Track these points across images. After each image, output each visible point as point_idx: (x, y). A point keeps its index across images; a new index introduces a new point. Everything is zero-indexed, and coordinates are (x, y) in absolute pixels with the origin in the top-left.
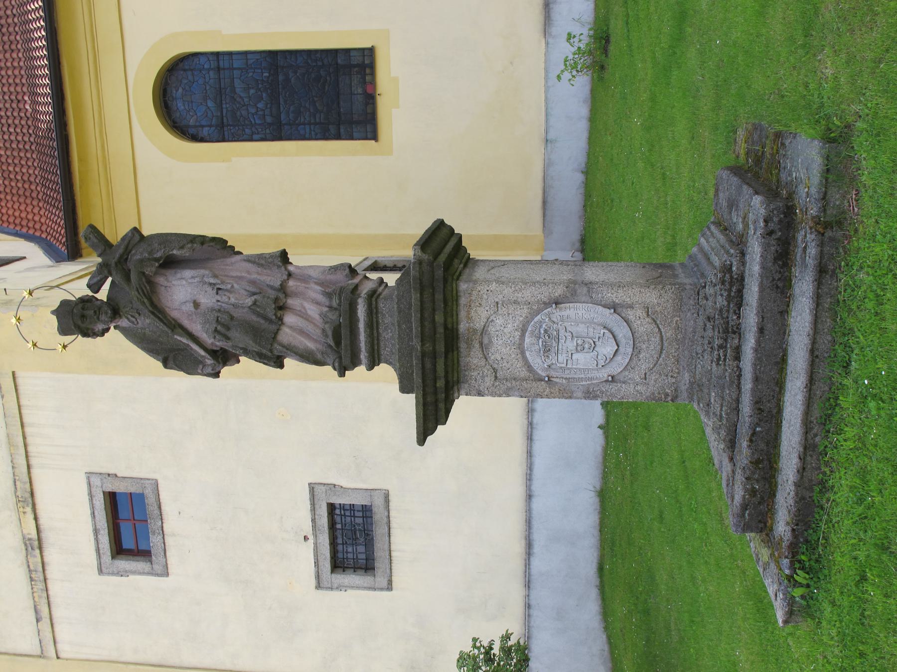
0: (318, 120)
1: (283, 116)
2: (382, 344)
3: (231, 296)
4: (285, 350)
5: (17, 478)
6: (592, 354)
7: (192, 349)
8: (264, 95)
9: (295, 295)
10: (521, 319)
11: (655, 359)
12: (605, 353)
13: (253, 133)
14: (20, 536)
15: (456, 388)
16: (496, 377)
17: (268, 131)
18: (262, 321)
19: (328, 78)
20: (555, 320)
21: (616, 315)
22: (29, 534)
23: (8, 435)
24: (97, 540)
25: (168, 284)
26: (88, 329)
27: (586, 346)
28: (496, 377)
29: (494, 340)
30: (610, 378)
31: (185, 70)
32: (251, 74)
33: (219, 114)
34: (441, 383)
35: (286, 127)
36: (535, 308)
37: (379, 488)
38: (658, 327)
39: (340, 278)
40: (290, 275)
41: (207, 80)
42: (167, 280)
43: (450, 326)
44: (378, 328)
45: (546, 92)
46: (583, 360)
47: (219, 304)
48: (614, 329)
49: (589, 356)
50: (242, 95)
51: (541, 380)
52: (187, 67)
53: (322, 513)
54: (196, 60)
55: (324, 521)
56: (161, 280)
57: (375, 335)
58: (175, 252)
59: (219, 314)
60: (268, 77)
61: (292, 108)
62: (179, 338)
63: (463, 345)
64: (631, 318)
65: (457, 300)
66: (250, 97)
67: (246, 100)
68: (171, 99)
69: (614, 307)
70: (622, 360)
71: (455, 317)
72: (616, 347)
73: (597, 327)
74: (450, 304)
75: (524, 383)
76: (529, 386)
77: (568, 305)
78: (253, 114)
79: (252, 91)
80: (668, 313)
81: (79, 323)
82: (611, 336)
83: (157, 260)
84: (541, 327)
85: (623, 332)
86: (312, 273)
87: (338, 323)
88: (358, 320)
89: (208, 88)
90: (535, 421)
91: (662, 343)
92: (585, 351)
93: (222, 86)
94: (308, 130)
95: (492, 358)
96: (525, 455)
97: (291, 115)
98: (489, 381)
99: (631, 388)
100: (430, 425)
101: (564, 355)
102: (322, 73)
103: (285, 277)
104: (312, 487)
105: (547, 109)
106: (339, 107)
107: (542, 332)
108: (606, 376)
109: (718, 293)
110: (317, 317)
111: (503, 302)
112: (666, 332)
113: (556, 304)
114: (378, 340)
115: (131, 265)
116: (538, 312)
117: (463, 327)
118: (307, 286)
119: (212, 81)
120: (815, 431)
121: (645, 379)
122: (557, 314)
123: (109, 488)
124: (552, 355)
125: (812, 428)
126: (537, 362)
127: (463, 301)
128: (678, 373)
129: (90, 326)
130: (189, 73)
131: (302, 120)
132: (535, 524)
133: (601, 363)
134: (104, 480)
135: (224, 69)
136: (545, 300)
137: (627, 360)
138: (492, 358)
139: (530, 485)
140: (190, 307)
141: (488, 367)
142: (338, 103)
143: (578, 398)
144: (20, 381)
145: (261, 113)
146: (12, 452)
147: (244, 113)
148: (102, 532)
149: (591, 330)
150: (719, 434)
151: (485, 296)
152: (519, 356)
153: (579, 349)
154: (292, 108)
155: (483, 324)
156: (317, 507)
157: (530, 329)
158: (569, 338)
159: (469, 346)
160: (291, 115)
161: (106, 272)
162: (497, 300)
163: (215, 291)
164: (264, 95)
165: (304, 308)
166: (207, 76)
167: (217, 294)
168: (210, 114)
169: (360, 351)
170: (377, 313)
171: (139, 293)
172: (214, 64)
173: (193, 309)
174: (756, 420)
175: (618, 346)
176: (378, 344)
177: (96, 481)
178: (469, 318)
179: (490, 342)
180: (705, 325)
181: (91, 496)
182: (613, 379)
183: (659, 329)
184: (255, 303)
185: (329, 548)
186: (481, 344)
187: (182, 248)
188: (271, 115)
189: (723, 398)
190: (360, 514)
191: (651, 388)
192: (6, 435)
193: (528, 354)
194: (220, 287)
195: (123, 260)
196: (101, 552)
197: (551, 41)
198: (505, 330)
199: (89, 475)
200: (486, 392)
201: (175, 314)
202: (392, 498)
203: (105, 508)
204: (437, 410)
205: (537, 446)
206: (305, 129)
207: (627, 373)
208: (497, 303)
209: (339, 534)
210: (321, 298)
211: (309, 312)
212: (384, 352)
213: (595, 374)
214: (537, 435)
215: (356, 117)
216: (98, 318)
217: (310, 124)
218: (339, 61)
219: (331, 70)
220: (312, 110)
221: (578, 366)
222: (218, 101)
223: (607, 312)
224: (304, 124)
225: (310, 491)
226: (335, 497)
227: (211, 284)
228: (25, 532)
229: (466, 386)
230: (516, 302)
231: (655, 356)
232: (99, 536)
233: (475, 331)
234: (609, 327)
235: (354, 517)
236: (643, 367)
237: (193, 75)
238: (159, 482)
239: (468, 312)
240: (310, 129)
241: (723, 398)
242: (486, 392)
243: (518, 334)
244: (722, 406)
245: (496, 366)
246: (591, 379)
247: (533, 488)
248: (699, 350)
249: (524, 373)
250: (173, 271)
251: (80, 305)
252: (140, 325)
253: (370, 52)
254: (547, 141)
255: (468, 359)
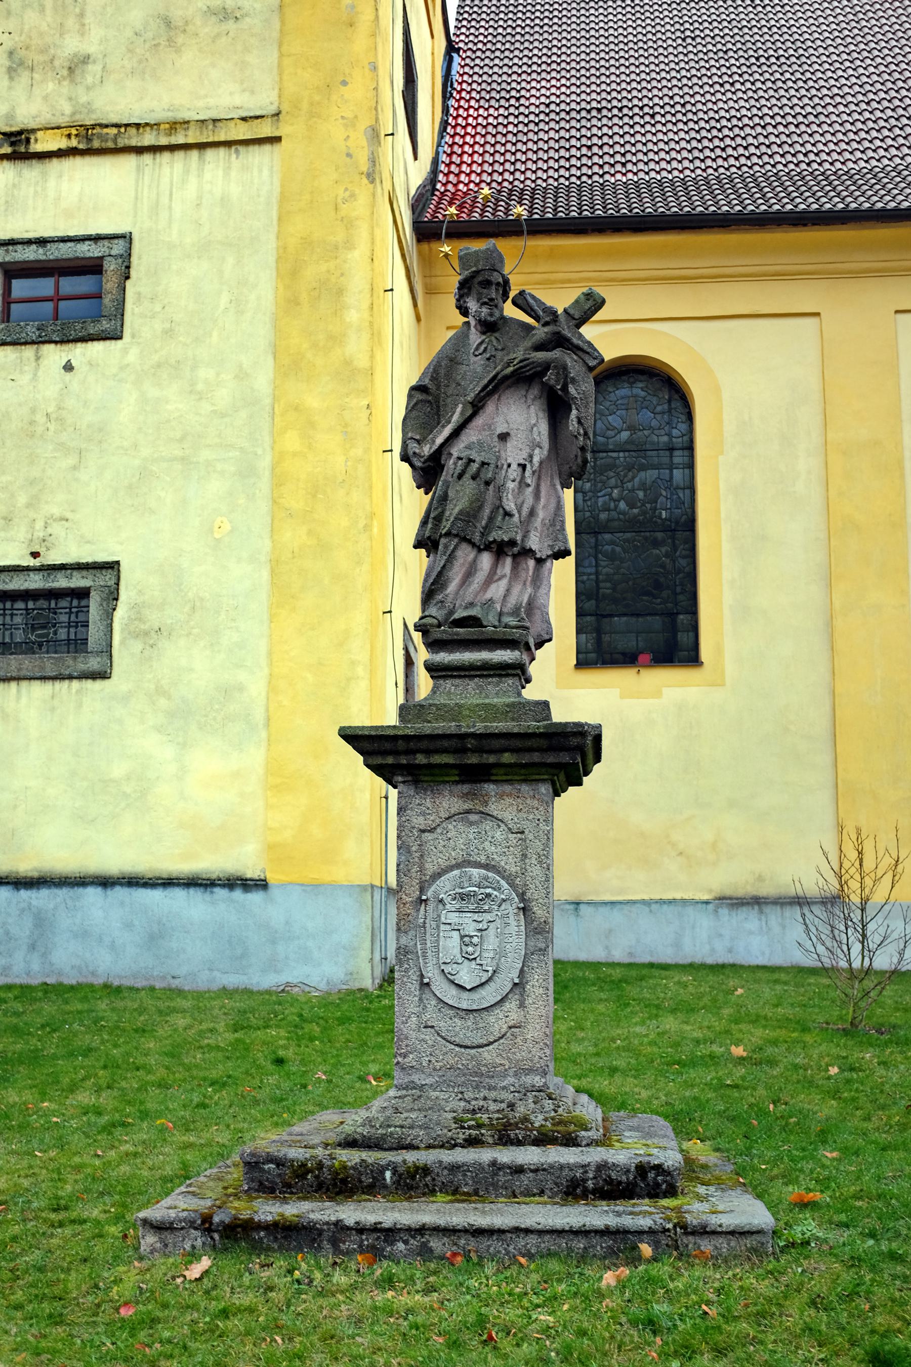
0: (602, 585)
1: (607, 536)
2: (457, 681)
3: (516, 483)
4: (448, 553)
5: (123, 130)
6: (459, 956)
7: (444, 427)
8: (636, 511)
9: (515, 567)
10: (503, 863)
11: (453, 1039)
12: (461, 974)
13: (584, 493)
14: (32, 125)
15: (410, 778)
16: (423, 831)
17: (588, 514)
18: (484, 523)
19: (659, 601)
20: (503, 907)
21: (510, 986)
22: (36, 140)
23: (188, 122)
24: (29, 242)
25: (529, 401)
26: (470, 289)
27: (470, 949)
28: (423, 831)
29: (474, 829)
30: (426, 981)
31: (669, 401)
32: (664, 493)
33: (611, 447)
34: (421, 759)
35: (593, 540)
36: (518, 881)
37: (114, 664)
38: (495, 1041)
39: (536, 628)
40: (540, 561)
41: (656, 432)
42: (533, 400)
43: (494, 771)
44: (480, 676)
45: (644, 902)
46: (451, 944)
47: (505, 467)
48: (492, 984)
49: (456, 951)
50: (637, 480)
51: (422, 890)
52: (673, 406)
53: (74, 579)
54: (683, 418)
55: (62, 582)
56: (535, 391)
57: (472, 673)
58: (574, 412)
59: (492, 466)
60: (660, 517)
61: (618, 549)
62: (459, 409)
63: (466, 788)
64: (507, 1005)
65: (525, 781)
66: (633, 490)
67: (630, 485)
68: (631, 380)
69: (519, 986)
70: (450, 995)
71: (505, 778)
72: (468, 987)
73: (495, 962)
74: (523, 771)
75: (416, 868)
76: (414, 875)
77: (523, 923)
78: (610, 495)
79: (641, 494)
80: (514, 1053)
81: (480, 278)
82: (483, 980)
83: (565, 388)
84: (494, 889)
85: (489, 995)
86: (542, 591)
87: (485, 623)
88: (491, 650)
89: (646, 432)
90: (217, 890)
91: (473, 1047)
92: (464, 948)
93: (649, 453)
94: (589, 570)
95: (450, 826)
96: (165, 876)
97: (608, 548)
98: (419, 822)
99: (413, 1008)
100: (367, 745)
101: (457, 920)
102: (665, 594)
103: (538, 556)
104: (113, 566)
105: (620, 903)
106: (619, 616)
107: (488, 891)
108: (430, 975)
109: (547, 1115)
110: (488, 595)
111: (524, 840)
112: (488, 1051)
113: (524, 909)
114: (465, 676)
115: (556, 354)
116: (512, 885)
117: (490, 788)
118: (528, 583)
119: (655, 438)
120: (412, 1241)
121: (425, 1027)
122: (510, 909)
123: (110, 266)
124: (457, 905)
125: (414, 1237)
126: (444, 886)
127: (525, 788)
128: (435, 1069)
129: (474, 291)
130: (666, 406)
131: (602, 563)
132: (63, 893)
133: (447, 969)
134: (120, 260)
135: (671, 456)
136: (528, 895)
137: (450, 1002)
138: (450, 826)
139: (121, 885)
140: (501, 429)
141: (438, 821)
142: (625, 615)
143: (398, 940)
144: (267, 148)
145: (612, 505)
146: (162, 127)
147: (613, 481)
148: (41, 251)
149: (491, 955)
150: (363, 1125)
151: (531, 817)
152: (454, 862)
153: (466, 939)
154: (618, 549)
155: (495, 813)
156: (84, 573)
157: (490, 874)
158: (480, 926)
159: (465, 796)
160: (608, 548)
161: (548, 319)
162: (527, 832)
163: (522, 462)
164: (636, 511)
165: (499, 579)
166: (663, 432)
167: (519, 465)
168: (610, 433)
169: (451, 652)
170: (500, 676)
171: (521, 361)
172: (678, 442)
173: (499, 431)
174: (401, 1169)
175: (470, 990)
176: (460, 677)
177: (118, 248)
178: (501, 796)
179: (472, 824)
180: (502, 1102)
181: (96, 238)
182: (425, 986)
183: (491, 1043)
184: (508, 514)
185: (22, 588)
186: (468, 812)
187: (579, 422)
188: (609, 520)
189: (411, 1127)
190: (72, 637)
191: (413, 1035)
192: (187, 119)
193: (456, 872)
194: (528, 467)
195: (559, 341)
196: (11, 248)
197: (711, 907)
198: (487, 843)
199: (127, 238)
200: (404, 819)
201: (490, 407)
202: (98, 685)
203: (77, 258)
204: (384, 753)
205: (179, 893)
206: (590, 566)
207: (434, 1002)
208: (522, 832)
209: (42, 603)
210: (512, 601)
211: (493, 587)
212: (448, 684)
213: (431, 961)
214: (195, 894)
215: (606, 638)
216: (485, 303)
217: (597, 573)
218: (681, 617)
219: (670, 605)
220: (616, 577)
221: (442, 939)
222: (628, 447)
223: (514, 975)
224: (597, 566)
225: (107, 563)
226: (99, 599)
227: (531, 456)
228: (40, 134)
229: (412, 792)
230: (524, 856)
231: (457, 1040)
232: (34, 247)
233: (486, 803)
234: (495, 978)
235: (69, 627)
236: (442, 1024)
237: (663, 413)
238: (119, 342)
239: (510, 795)
240: (590, 574)
241: (411, 1127)
242: (404, 819)
243: (483, 858)
244: (402, 1127)
245: (439, 830)
246: (425, 956)
247: (118, 889)
248: (469, 1095)
249: (430, 869)
250: (545, 407)
251: (501, 280)
252: (473, 359)
253: (692, 658)
254: (578, 904)
255: (446, 793)
